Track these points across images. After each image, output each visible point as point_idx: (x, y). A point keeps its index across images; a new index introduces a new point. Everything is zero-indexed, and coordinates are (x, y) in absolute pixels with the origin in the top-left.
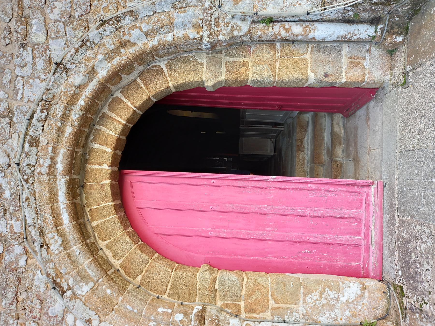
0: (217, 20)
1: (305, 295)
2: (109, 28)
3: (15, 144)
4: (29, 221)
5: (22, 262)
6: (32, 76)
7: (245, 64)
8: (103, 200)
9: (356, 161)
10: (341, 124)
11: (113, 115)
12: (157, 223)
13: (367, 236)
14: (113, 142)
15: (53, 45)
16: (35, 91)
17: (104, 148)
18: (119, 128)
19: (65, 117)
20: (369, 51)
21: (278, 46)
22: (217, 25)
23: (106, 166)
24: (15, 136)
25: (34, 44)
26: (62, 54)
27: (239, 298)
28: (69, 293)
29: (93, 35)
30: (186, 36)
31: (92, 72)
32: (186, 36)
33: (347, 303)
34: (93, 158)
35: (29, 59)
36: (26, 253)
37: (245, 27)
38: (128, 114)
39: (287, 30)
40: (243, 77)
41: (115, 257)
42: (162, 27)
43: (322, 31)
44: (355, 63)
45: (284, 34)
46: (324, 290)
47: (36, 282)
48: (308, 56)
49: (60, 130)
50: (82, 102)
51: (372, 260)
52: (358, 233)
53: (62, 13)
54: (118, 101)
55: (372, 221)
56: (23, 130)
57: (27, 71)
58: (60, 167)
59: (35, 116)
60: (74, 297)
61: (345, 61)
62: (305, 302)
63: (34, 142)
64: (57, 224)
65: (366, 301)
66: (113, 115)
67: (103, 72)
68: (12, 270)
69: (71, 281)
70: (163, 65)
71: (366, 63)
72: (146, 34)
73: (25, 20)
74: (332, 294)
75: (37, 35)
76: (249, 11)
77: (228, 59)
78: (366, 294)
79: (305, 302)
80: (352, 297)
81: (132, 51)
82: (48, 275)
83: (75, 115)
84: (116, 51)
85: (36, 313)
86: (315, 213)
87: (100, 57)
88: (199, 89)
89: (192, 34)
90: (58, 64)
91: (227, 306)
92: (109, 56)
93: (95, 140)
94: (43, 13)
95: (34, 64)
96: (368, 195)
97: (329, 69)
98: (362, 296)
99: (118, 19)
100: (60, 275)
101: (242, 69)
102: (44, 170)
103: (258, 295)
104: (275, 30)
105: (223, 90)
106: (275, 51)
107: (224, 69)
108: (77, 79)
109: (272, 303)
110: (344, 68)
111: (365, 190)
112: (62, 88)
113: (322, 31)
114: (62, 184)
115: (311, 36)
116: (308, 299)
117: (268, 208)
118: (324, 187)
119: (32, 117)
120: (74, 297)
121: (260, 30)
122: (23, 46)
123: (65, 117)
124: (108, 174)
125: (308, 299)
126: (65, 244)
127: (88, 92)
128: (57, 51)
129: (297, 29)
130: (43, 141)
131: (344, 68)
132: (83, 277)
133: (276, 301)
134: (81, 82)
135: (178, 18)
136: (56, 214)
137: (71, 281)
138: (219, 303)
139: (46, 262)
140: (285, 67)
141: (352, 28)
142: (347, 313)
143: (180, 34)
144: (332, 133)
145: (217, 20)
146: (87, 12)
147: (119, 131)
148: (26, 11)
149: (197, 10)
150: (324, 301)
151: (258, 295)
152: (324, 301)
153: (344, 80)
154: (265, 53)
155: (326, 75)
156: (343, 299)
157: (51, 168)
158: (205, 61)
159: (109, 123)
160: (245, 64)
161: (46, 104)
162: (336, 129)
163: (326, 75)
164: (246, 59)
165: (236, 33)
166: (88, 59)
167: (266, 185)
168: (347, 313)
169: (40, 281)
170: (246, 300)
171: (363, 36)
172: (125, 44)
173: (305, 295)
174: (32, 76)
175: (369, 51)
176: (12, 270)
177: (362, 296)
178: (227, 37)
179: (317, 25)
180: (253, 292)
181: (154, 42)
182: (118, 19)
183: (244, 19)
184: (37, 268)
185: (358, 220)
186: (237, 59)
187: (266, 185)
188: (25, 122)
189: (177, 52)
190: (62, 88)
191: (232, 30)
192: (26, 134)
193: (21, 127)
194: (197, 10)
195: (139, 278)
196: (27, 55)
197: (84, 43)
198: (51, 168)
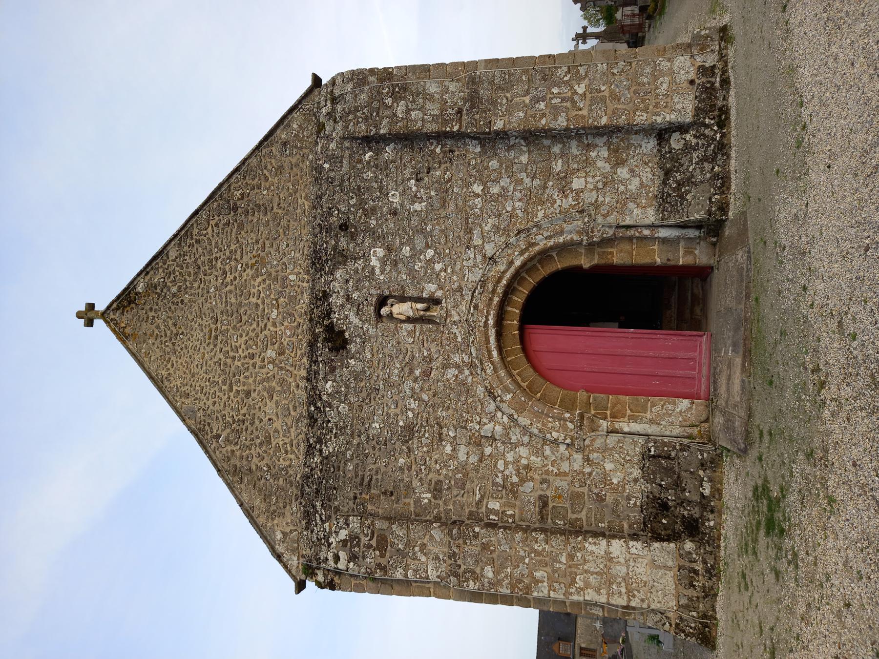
0: (592, 229)
1: (651, 407)
2: (523, 235)
3: (464, 308)
4: (474, 355)
5: (470, 380)
6: (474, 266)
7: (611, 253)
8: (515, 344)
9: (707, 318)
10: (700, 286)
11: (520, 288)
12: (547, 361)
13: (700, 371)
14: (520, 306)
15: (487, 246)
16: (475, 276)
17: (514, 310)
18: (524, 297)
19: (494, 292)
20: (699, 243)
21: (635, 241)
22: (592, 232)
23: (515, 322)
24: (464, 303)
25: (475, 246)
26: (493, 253)
27: (606, 409)
28: (499, 399)
29: (513, 240)
30: (572, 239)
31: (511, 263)
32: (572, 239)
33: (681, 412)
34: (507, 316)
35: (472, 255)
36: (472, 374)
37: (611, 232)
38: (530, 287)
39: (640, 233)
40: (610, 262)
41: (523, 381)
42: (557, 233)
43: (663, 233)
44: (689, 252)
45: (637, 234)
46: (664, 404)
47: (478, 392)
48: (656, 247)
49: (491, 299)
50: (504, 282)
51: (703, 388)
52: (694, 369)
53: (493, 226)
54: (524, 279)
55: (703, 361)
56: (469, 299)
57: (471, 263)
58: (491, 322)
59: (477, 291)
60: (502, 401)
61: (682, 251)
62: (651, 412)
63: (476, 307)
64: (490, 356)
65: (693, 411)
66: (520, 288)
67: (518, 263)
68: (464, 385)
69: (499, 392)
70: (554, 254)
71: (697, 252)
72: (546, 238)
73: (469, 231)
74: (670, 407)
75: (477, 241)
76: (614, 224)
77: (600, 250)
78: (694, 407)
79: (651, 412)
80: (684, 409)
81: (537, 248)
82: (486, 387)
83: (500, 290)
84: (527, 249)
85: (479, 410)
86: (662, 355)
87: (516, 253)
88: (579, 268)
89: (576, 238)
90: (490, 259)
91: (598, 413)
92: (522, 253)
93: (508, 305)
94: (481, 226)
95: (475, 258)
96: (701, 342)
97: (670, 256)
98: (691, 408)
99: (529, 230)
100: (493, 388)
101: (609, 257)
102: (482, 324)
103: (619, 407)
104: (631, 233)
105: (594, 268)
106: (633, 244)
107: (596, 256)
108: (502, 268)
109: (629, 412)
110: (681, 255)
111: (699, 338)
112: (493, 273)
113: (663, 233)
114: (492, 333)
115: (656, 235)
116: (653, 410)
117: (627, 351)
118: (669, 337)
119: (474, 291)
120: (502, 401)
121: (621, 233)
122: (468, 247)
123: (494, 292)
124: (517, 327)
125: (653, 410)
126: (495, 370)
127: (508, 275)
128: (489, 249)
129: (646, 232)
130: (481, 306)
131: (681, 255)
132: (507, 390)
133: (632, 411)
134: (504, 270)
135: (567, 227)
136: (489, 352)
137: (499, 392)
138: (593, 412)
139: (484, 380)
140: (639, 255)
141: (684, 231)
142: (680, 419)
143: (568, 238)
144: (693, 294)
145: (592, 229)
146: (508, 225)
147: (524, 299)
148: (470, 225)
149: (580, 223)
150: (664, 411)
151: (619, 407)
152: (664, 411)
153: (681, 263)
154: (626, 247)
155: (668, 260)
156: (678, 410)
157: (486, 322)
158: (583, 251)
159: (518, 293)
160: (611, 253)
161: (483, 283)
162: (696, 291)
163: (668, 260)
164: (612, 250)
165: (605, 236)
166: (509, 255)
167: (627, 335)
168: (680, 419)
169: (480, 391)
170: (611, 410)
171: (692, 236)
172: (533, 245)
173: (651, 407)
174: (474, 266)
175: (699, 243)
176: (464, 385)
177: (691, 408)
178: (599, 239)
179: (660, 229)
180: (616, 404)
181: (551, 243)
182: (529, 230)
183: (610, 227)
184: (478, 384)
185: (694, 360)
186: (606, 250)
187: (627, 335)
188: (470, 294)
189: (564, 248)
190: (493, 273)
191: (603, 234)
192: (471, 302)
193: (468, 298)
194: (580, 223)
195: (539, 395)
196: (471, 253)
197: (507, 245)
198: (486, 322)
